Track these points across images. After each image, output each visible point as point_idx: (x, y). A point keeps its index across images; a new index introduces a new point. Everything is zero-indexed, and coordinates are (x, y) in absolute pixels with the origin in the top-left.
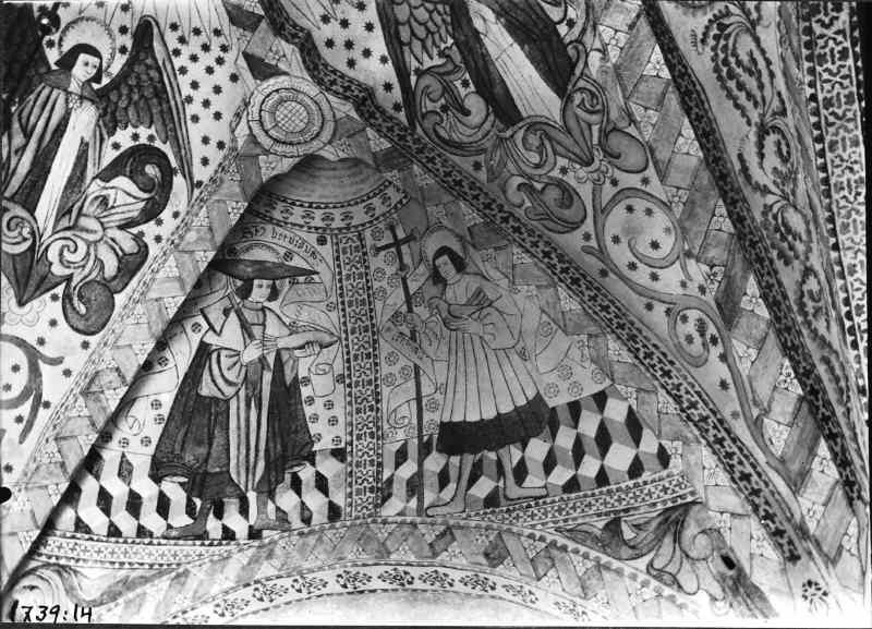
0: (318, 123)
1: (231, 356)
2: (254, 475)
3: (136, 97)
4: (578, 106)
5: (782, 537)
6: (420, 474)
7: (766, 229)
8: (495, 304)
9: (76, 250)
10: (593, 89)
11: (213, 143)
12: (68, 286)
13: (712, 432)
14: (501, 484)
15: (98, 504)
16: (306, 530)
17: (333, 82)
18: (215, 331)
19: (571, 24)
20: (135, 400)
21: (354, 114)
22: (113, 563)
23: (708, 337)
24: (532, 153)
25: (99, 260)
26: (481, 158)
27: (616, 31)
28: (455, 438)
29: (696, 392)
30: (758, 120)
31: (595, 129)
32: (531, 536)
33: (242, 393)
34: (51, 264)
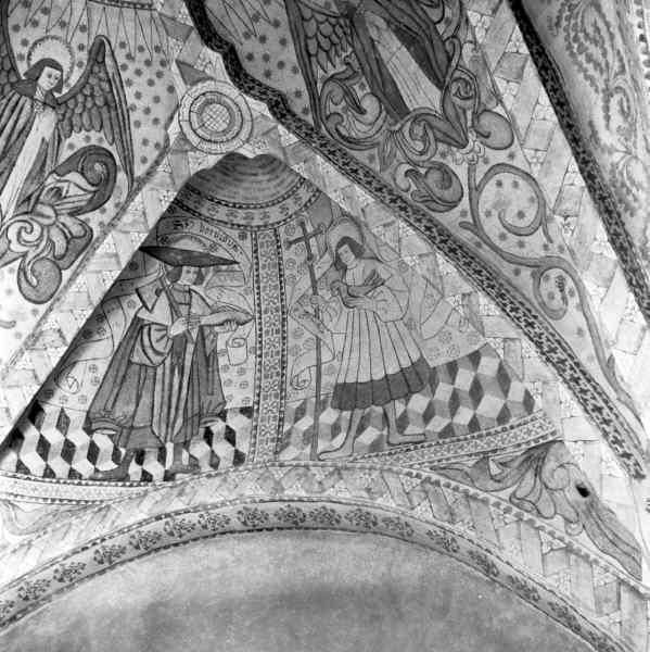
0: (238, 123)
1: (159, 330)
2: (173, 429)
3: (89, 105)
4: (455, 95)
5: (629, 458)
6: (315, 426)
7: (614, 186)
8: (387, 283)
9: (32, 231)
10: (468, 78)
11: (151, 144)
12: (23, 261)
13: (569, 372)
14: (385, 433)
15: (37, 450)
16: (213, 473)
17: (251, 88)
18: (147, 308)
19: (448, 22)
20: (75, 363)
21: (268, 113)
22: (46, 499)
23: (567, 291)
24: (417, 142)
25: (51, 241)
26: (375, 151)
27: (482, 15)
28: (348, 396)
29: (557, 341)
30: (604, 86)
31: (469, 113)
32: (409, 474)
33: (168, 362)
34: (10, 242)
